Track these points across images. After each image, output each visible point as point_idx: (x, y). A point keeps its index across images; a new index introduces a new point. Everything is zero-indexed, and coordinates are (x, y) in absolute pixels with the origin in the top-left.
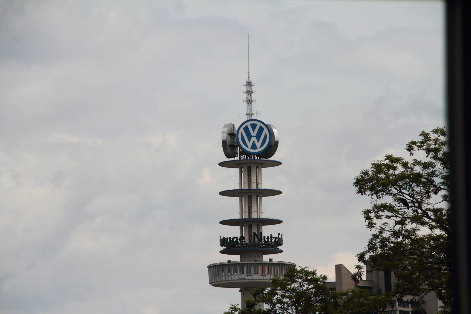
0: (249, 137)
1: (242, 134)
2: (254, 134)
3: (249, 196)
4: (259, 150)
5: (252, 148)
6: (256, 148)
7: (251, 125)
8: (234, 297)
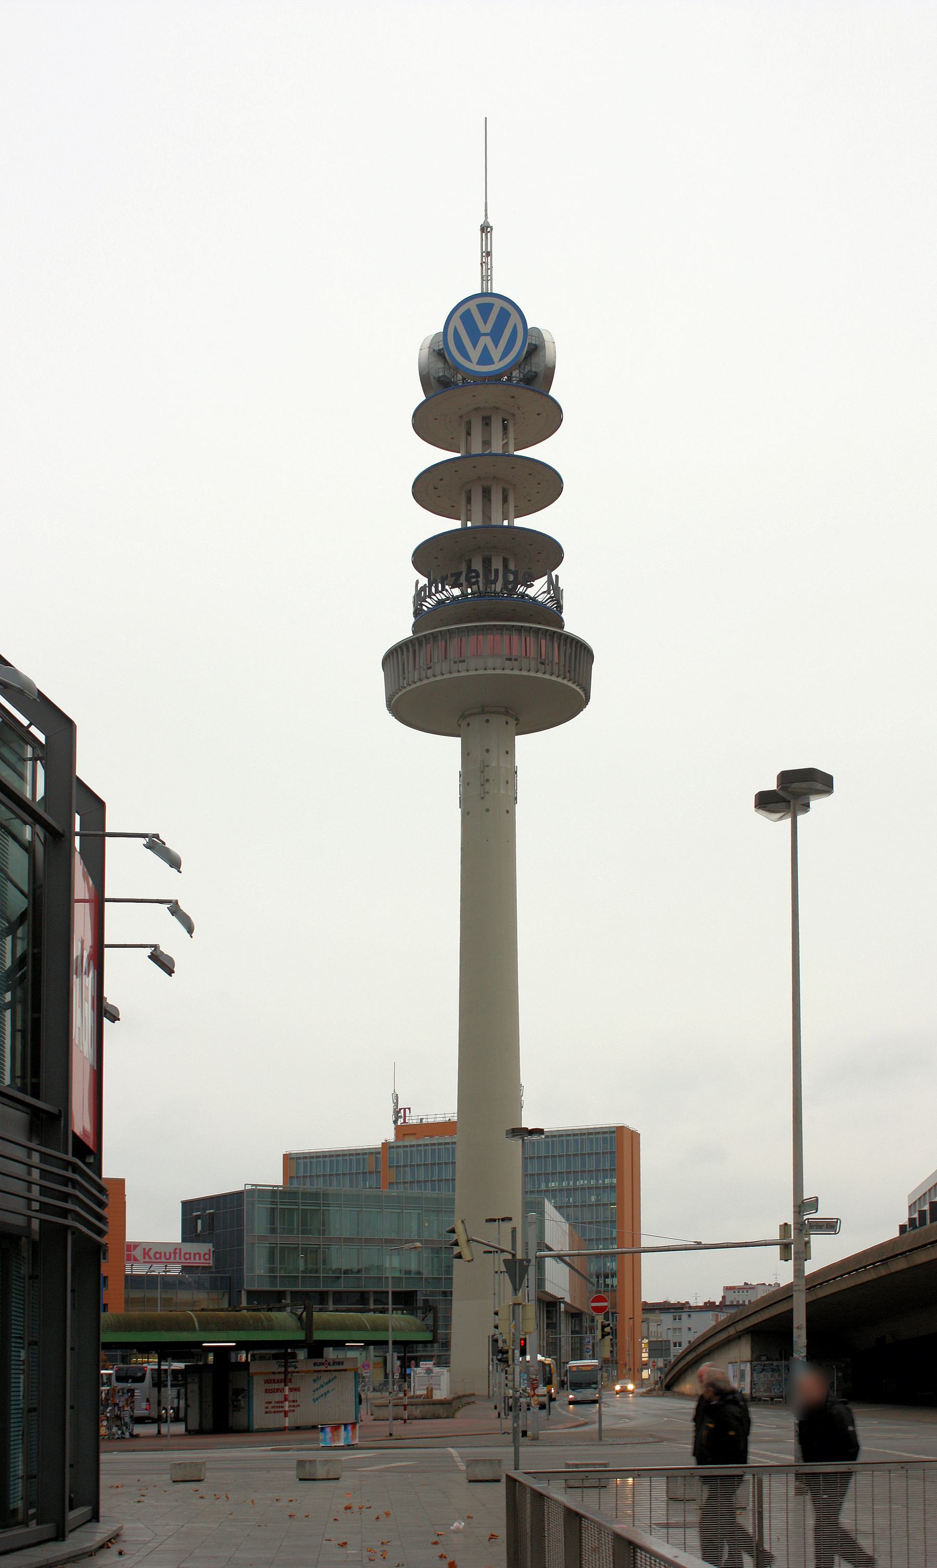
0: (475, 336)
1: (455, 329)
2: (485, 328)
3: (484, 418)
4: (497, 366)
5: (480, 363)
6: (491, 362)
7: (479, 306)
8: (878, 1433)
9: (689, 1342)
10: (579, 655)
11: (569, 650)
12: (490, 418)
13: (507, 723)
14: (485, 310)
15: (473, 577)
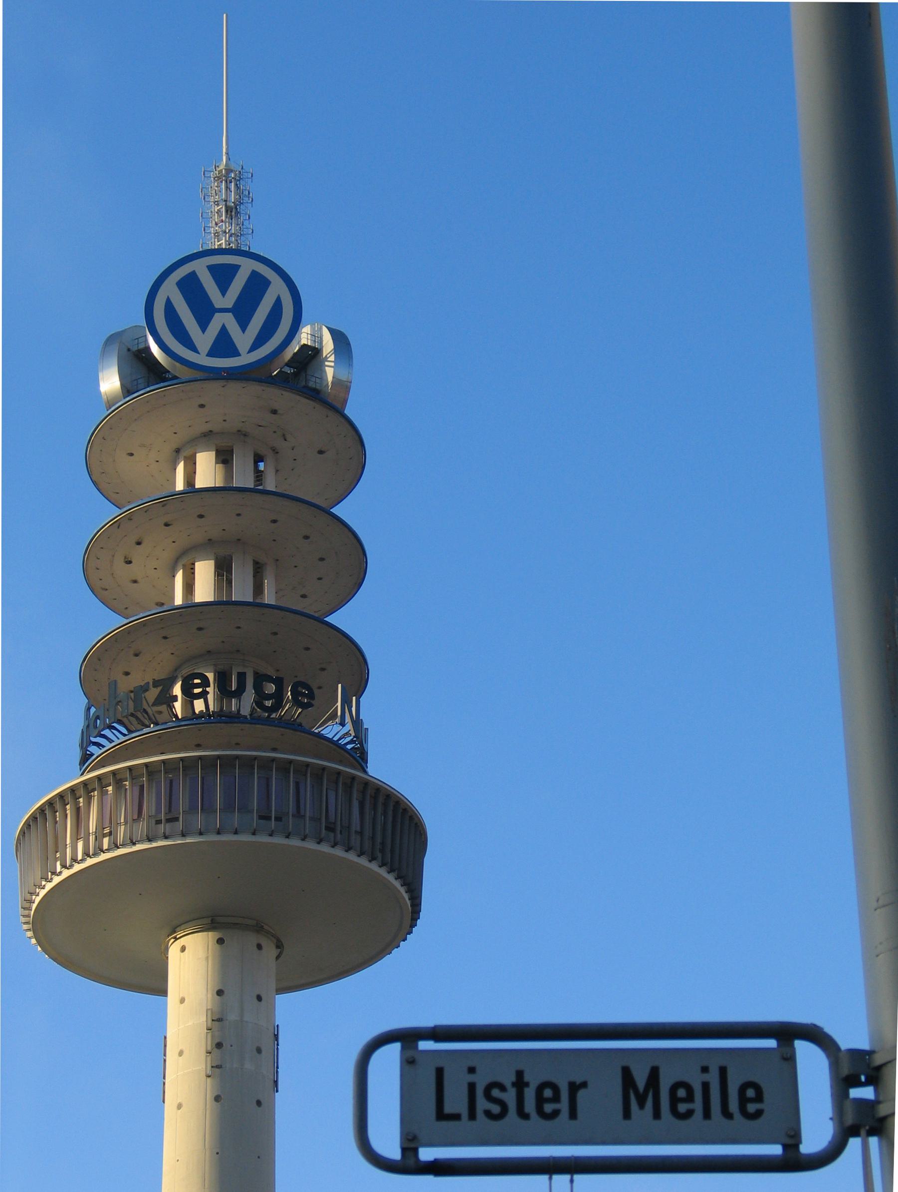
0: (204, 311)
5: (211, 354)
9: (831, 1119)
10: (393, 834)
11: (380, 819)
12: (231, 452)
13: (259, 947)
14: (223, 275)
15: (197, 686)
